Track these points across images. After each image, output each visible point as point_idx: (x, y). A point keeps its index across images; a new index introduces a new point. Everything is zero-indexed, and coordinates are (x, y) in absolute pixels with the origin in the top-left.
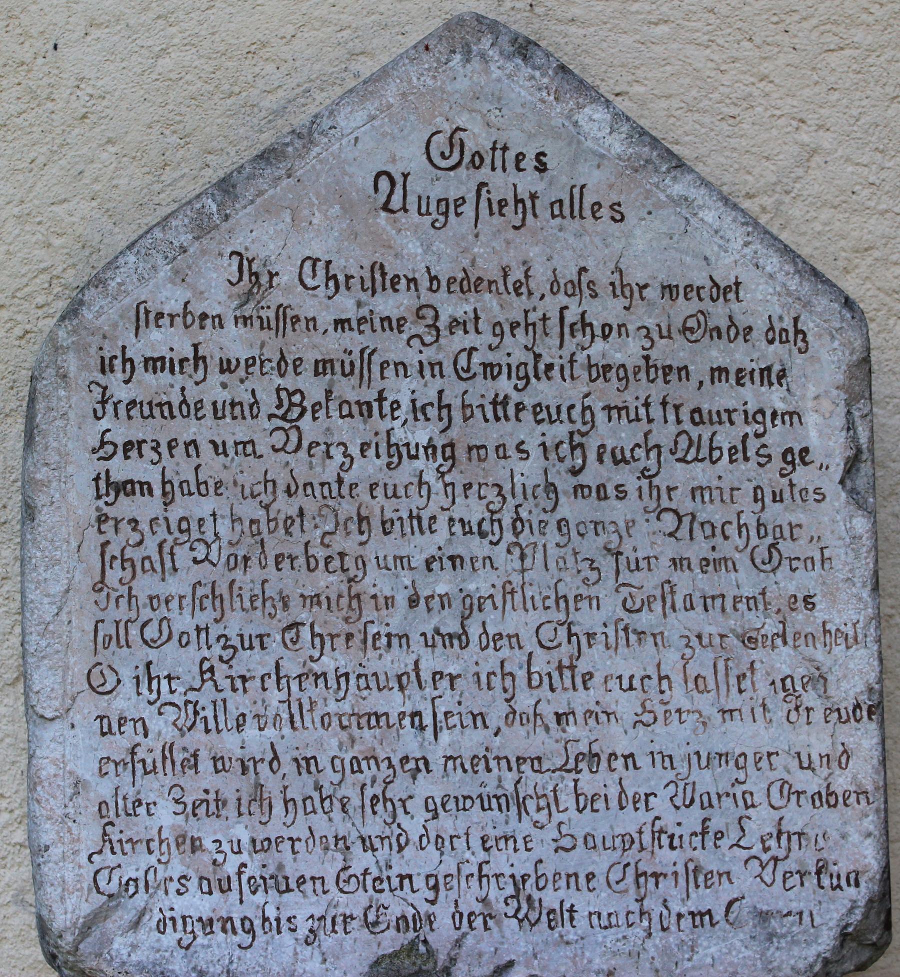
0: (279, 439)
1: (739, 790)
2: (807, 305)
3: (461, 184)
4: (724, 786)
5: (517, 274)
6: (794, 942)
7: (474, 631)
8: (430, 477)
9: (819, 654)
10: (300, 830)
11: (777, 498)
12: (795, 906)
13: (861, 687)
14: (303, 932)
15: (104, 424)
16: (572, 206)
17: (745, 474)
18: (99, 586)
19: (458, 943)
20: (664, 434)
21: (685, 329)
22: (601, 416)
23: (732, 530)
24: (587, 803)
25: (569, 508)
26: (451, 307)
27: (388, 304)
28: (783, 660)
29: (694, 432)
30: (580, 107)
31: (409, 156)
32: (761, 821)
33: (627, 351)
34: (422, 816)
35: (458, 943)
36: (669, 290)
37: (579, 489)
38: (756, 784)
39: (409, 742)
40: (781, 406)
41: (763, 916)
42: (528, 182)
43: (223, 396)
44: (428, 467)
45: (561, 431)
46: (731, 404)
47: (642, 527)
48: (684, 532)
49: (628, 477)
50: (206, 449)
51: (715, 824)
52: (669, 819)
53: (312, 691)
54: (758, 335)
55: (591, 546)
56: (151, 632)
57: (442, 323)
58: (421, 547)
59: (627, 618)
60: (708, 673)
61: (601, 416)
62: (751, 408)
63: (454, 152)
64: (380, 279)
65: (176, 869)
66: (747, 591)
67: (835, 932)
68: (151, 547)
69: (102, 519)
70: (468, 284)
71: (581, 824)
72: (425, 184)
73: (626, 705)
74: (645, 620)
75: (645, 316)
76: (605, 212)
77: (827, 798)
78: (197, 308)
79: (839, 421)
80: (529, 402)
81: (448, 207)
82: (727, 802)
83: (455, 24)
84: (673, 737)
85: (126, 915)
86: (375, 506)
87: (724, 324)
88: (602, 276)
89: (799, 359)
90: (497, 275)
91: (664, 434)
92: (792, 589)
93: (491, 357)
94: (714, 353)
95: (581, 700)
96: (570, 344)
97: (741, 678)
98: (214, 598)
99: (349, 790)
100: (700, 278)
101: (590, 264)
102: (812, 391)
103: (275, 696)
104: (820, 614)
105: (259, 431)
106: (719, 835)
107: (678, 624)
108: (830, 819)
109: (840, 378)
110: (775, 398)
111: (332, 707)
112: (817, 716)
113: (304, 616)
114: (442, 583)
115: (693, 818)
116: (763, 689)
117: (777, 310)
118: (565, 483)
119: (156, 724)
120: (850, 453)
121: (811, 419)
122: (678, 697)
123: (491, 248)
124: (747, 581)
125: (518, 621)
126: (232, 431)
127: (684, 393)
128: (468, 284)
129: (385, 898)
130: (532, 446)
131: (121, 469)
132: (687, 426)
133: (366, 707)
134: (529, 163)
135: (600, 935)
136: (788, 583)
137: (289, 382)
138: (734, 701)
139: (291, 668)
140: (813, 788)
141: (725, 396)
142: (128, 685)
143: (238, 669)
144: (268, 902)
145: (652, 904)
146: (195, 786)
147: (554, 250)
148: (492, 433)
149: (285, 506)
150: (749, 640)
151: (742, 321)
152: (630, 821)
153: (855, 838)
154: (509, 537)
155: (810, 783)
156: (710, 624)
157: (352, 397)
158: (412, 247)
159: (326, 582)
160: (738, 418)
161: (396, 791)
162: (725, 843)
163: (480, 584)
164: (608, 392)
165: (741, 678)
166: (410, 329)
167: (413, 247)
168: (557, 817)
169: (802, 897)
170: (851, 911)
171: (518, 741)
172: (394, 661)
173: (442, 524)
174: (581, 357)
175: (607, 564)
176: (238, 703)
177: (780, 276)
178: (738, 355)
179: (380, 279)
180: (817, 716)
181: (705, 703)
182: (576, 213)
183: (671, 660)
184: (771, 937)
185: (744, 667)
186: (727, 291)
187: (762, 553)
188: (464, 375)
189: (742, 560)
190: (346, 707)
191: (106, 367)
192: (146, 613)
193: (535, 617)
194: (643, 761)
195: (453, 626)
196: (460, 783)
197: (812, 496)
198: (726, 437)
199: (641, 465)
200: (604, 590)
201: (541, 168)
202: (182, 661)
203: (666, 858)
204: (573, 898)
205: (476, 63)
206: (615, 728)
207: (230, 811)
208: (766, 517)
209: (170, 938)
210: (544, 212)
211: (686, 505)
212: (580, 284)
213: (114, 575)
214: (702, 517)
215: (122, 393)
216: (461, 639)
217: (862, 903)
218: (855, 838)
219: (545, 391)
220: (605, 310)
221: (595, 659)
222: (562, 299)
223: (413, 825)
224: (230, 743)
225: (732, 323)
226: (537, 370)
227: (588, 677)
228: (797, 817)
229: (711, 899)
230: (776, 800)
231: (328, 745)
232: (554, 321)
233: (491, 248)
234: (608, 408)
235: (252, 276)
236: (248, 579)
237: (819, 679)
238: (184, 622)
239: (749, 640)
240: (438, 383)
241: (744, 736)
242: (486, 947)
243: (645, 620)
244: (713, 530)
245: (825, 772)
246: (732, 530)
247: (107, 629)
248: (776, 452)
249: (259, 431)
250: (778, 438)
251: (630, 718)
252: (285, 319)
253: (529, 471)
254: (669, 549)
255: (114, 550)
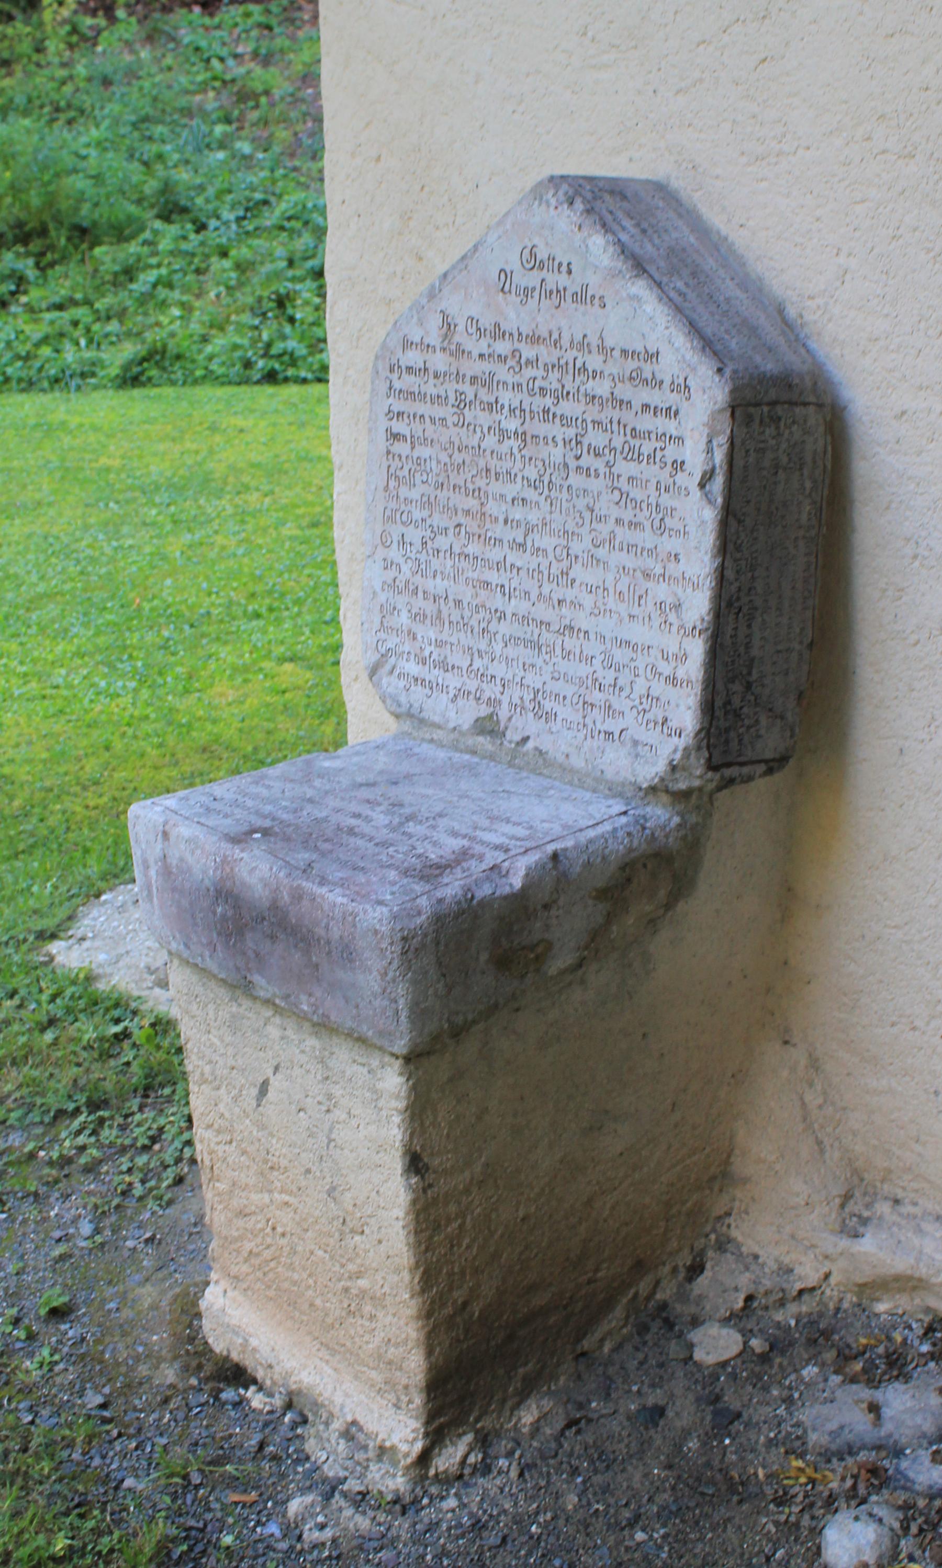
0: (456, 418)
1: (633, 665)
2: (694, 369)
3: (532, 280)
4: (626, 661)
5: (555, 336)
6: (646, 762)
7: (529, 544)
8: (515, 450)
9: (680, 591)
10: (454, 640)
11: (667, 490)
12: (650, 741)
13: (697, 617)
14: (451, 695)
15: (391, 400)
16: (581, 297)
17: (651, 472)
18: (386, 488)
19: (510, 719)
20: (618, 442)
21: (631, 378)
22: (590, 426)
23: (644, 506)
24: (567, 655)
25: (575, 480)
26: (528, 352)
27: (503, 347)
28: (661, 591)
29: (632, 442)
30: (590, 236)
31: (513, 263)
32: (641, 686)
33: (602, 388)
34: (501, 645)
35: (510, 719)
36: (624, 352)
37: (578, 468)
38: (641, 663)
39: (498, 602)
40: (674, 433)
41: (636, 743)
42: (563, 280)
43: (434, 392)
44: (514, 443)
45: (571, 432)
46: (651, 428)
47: (604, 497)
48: (623, 502)
49: (599, 464)
50: (428, 420)
51: (620, 682)
52: (600, 674)
53: (464, 564)
54: (666, 385)
55: (581, 503)
56: (404, 517)
57: (523, 361)
58: (511, 490)
59: (593, 550)
60: (625, 590)
61: (590, 426)
62: (660, 432)
63: (534, 262)
64: (498, 333)
65: (407, 648)
66: (649, 545)
67: (666, 762)
68: (405, 472)
69: (388, 452)
70: (535, 339)
71: (564, 666)
72: (523, 279)
73: (588, 601)
74: (601, 552)
75: (612, 368)
76: (596, 301)
77: (672, 680)
78: (426, 341)
79: (702, 446)
80: (559, 413)
81: (527, 292)
82: (627, 670)
83: (552, 179)
84: (606, 625)
85: (388, 667)
86: (493, 463)
87: (650, 377)
88: (594, 340)
89: (685, 404)
90: (546, 335)
91: (618, 442)
92: (669, 548)
93: (544, 384)
94: (644, 395)
95: (570, 594)
96: (578, 380)
97: (640, 597)
98: (428, 503)
99: (474, 622)
100: (640, 348)
101: (589, 333)
102: (690, 426)
103: (449, 563)
104: (682, 566)
105: (447, 411)
106: (621, 689)
107: (619, 558)
108: (671, 693)
109: (705, 419)
110: (671, 427)
111: (470, 574)
112: (674, 629)
113: (463, 521)
114: (517, 513)
115: (610, 675)
116: (650, 607)
117: (676, 371)
118: (573, 464)
119: (405, 568)
120: (708, 468)
121: (688, 443)
122: (611, 602)
123: (543, 317)
124: (646, 538)
125: (547, 542)
126: (438, 412)
127: (628, 417)
128: (535, 339)
129: (484, 685)
130: (559, 439)
131: (399, 427)
132: (629, 437)
133: (483, 578)
134: (564, 268)
135: (566, 732)
136: (669, 544)
137: (460, 387)
138: (636, 611)
139: (456, 549)
140: (666, 673)
141: (646, 422)
142: (395, 545)
143: (436, 546)
144: (436, 674)
145: (588, 721)
146: (419, 603)
147: (575, 322)
148: (542, 429)
149: (458, 458)
150: (647, 575)
151: (659, 376)
152: (583, 670)
153: (682, 708)
154: (546, 492)
155: (666, 669)
156: (630, 561)
157: (485, 399)
158: (515, 316)
159: (472, 503)
160: (653, 436)
161: (493, 627)
162: (624, 694)
163: (534, 517)
164: (593, 413)
165: (640, 597)
166: (511, 363)
167: (512, 315)
168: (554, 660)
169: (652, 736)
170: (675, 751)
171: (543, 612)
172: (495, 554)
173: (519, 479)
174: (582, 389)
175: (587, 515)
176: (436, 563)
177: (683, 350)
178: (655, 397)
179: (498, 333)
180: (674, 629)
181: (622, 608)
182: (583, 301)
183: (610, 578)
184: (637, 756)
185: (643, 592)
186: (652, 356)
187: (657, 523)
188: (531, 393)
189: (647, 524)
190: (475, 575)
191: (392, 370)
192: (403, 507)
193: (554, 541)
194: (592, 636)
195: (520, 540)
196: (516, 630)
197: (683, 492)
198: (647, 448)
199: (607, 458)
200: (584, 531)
201: (570, 272)
202: (414, 535)
203: (597, 697)
204: (558, 708)
205: (544, 206)
206: (582, 614)
207: (428, 622)
208: (661, 500)
209: (402, 683)
210: (569, 299)
211: (625, 487)
212: (583, 345)
213: (392, 483)
214: (631, 495)
215: (397, 385)
216: (522, 546)
217: (681, 748)
218: (682, 708)
219: (567, 408)
220: (594, 362)
221: (577, 571)
222: (575, 353)
223: (498, 647)
224: (430, 585)
225: (654, 377)
226: (562, 395)
227: (573, 581)
228: (658, 687)
229: (613, 725)
230: (650, 677)
231: (467, 595)
232: (571, 366)
233: (543, 317)
234: (593, 422)
235: (449, 327)
236: (443, 495)
237: (677, 607)
238: (417, 515)
239: (647, 575)
240: (519, 397)
241: (638, 633)
242: (520, 725)
243: (601, 552)
244: (637, 505)
245: (673, 664)
246: (644, 506)
247: (388, 513)
248: (670, 461)
249: (447, 411)
250: (671, 453)
251: (588, 610)
252: (460, 352)
253: (557, 453)
254: (615, 512)
255: (392, 470)
